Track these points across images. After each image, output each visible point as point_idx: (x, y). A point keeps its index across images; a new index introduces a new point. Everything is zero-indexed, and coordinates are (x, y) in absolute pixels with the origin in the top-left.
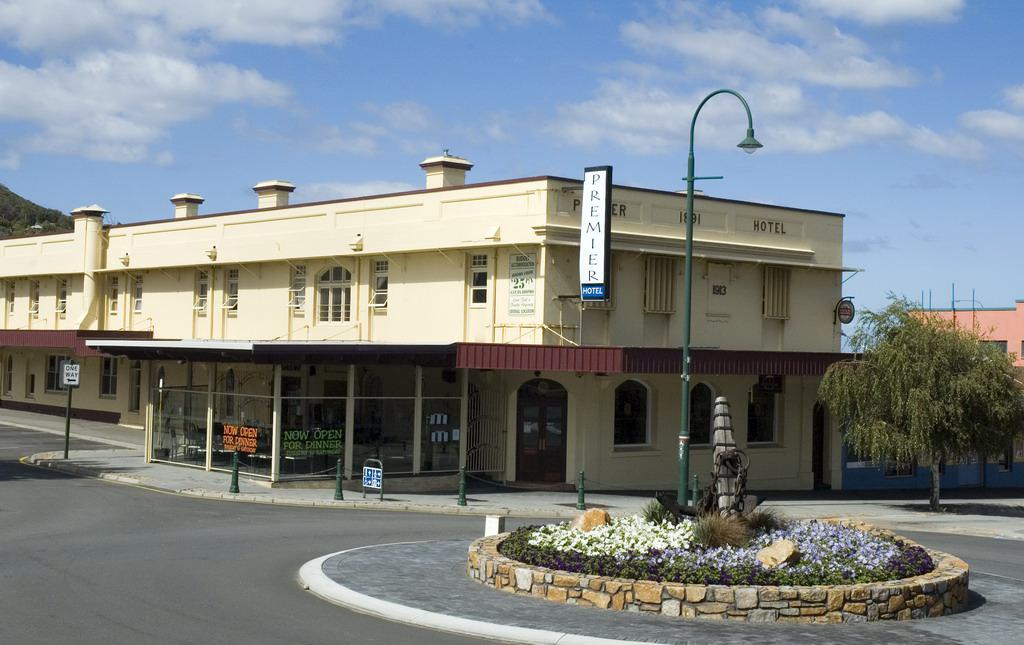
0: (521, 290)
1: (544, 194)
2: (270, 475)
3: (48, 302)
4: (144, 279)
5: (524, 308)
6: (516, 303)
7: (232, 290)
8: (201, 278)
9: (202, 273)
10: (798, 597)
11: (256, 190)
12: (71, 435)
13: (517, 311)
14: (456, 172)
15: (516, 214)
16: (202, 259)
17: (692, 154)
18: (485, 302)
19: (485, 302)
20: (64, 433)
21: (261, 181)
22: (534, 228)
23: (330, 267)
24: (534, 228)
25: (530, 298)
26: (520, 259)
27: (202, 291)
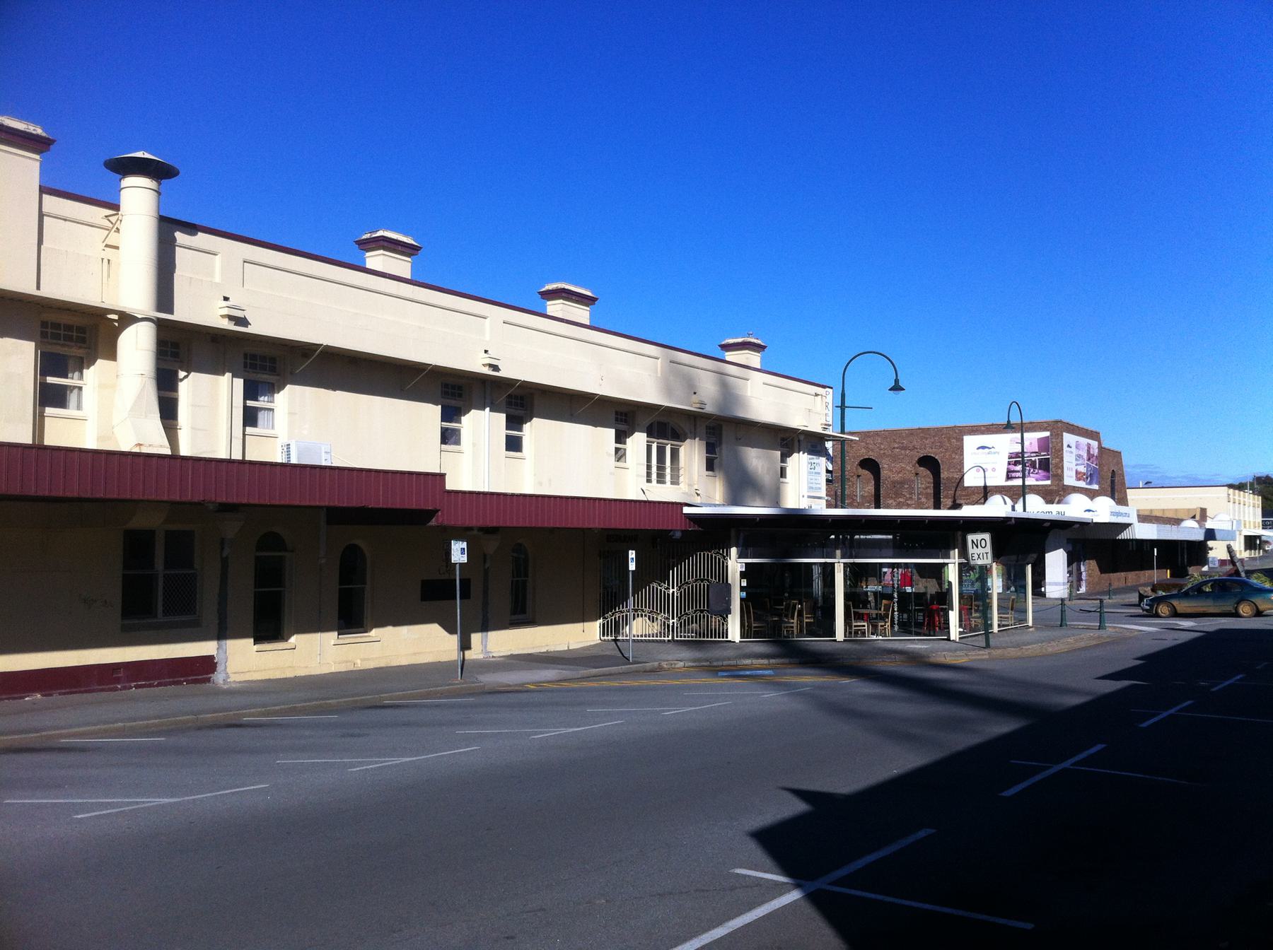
3: (483, 425)
8: (454, 392)
16: (477, 365)
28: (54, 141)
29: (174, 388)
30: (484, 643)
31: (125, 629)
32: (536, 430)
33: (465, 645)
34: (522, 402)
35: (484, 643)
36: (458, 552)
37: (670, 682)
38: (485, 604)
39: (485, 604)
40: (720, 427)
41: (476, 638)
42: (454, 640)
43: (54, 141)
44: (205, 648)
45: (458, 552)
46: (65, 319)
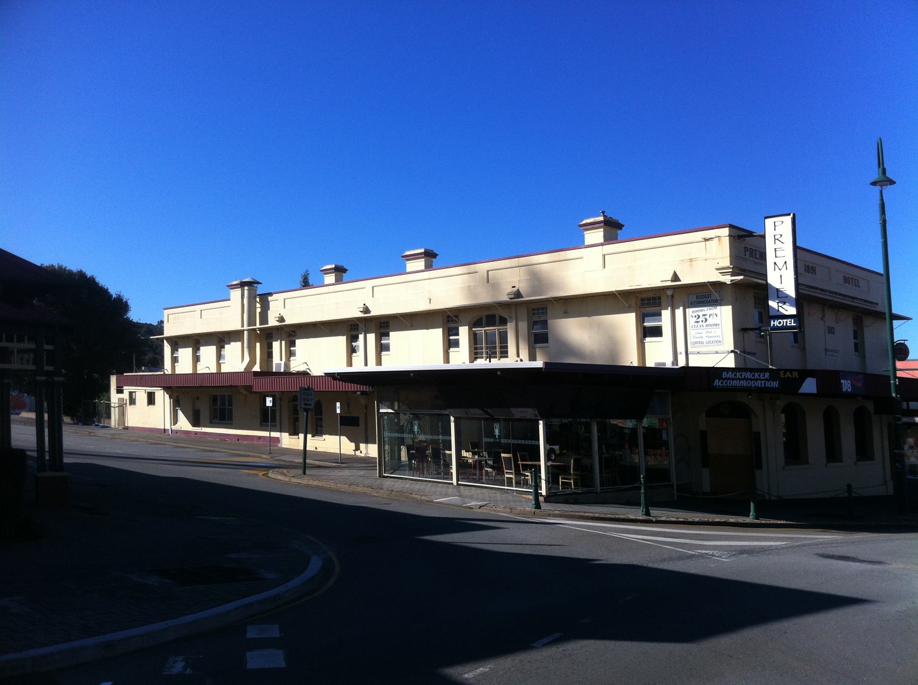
0: (704, 324)
1: (726, 241)
2: (452, 479)
3: (208, 353)
4: (549, 311)
5: (709, 339)
6: (699, 335)
7: (196, 350)
8: (350, 329)
9: (448, 317)
10: (350, 485)
11: (581, 226)
12: (307, 461)
13: (702, 343)
14: (613, 230)
15: (704, 256)
16: (355, 313)
17: (882, 200)
18: (661, 335)
19: (661, 335)
20: (301, 460)
21: (587, 218)
22: (717, 269)
23: (484, 314)
24: (717, 269)
25: (717, 332)
26: (702, 295)
27: (353, 338)
28: (894, 183)
29: (272, 348)
30: (367, 448)
31: (211, 423)
32: (396, 338)
33: (357, 448)
34: (383, 326)
35: (367, 448)
36: (269, 402)
37: (779, 543)
38: (366, 430)
39: (366, 430)
40: (388, 322)
41: (362, 446)
42: (352, 446)
43: (894, 183)
44: (275, 434)
45: (269, 402)
46: (650, 295)
